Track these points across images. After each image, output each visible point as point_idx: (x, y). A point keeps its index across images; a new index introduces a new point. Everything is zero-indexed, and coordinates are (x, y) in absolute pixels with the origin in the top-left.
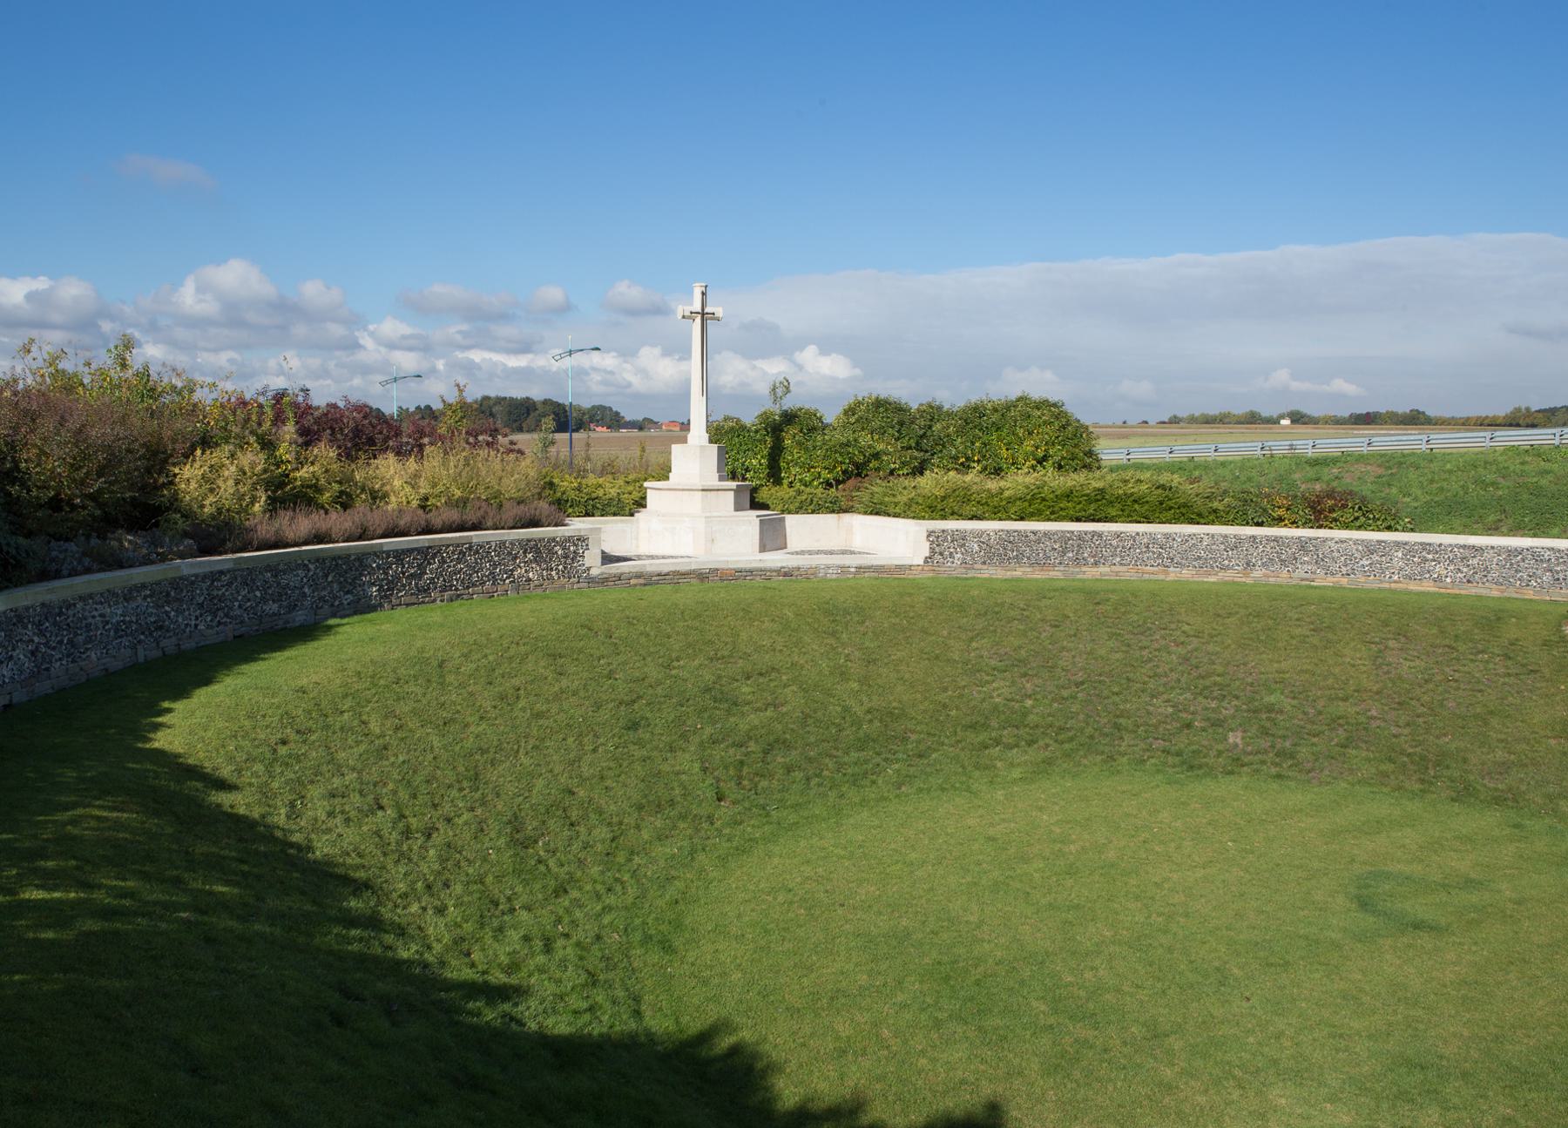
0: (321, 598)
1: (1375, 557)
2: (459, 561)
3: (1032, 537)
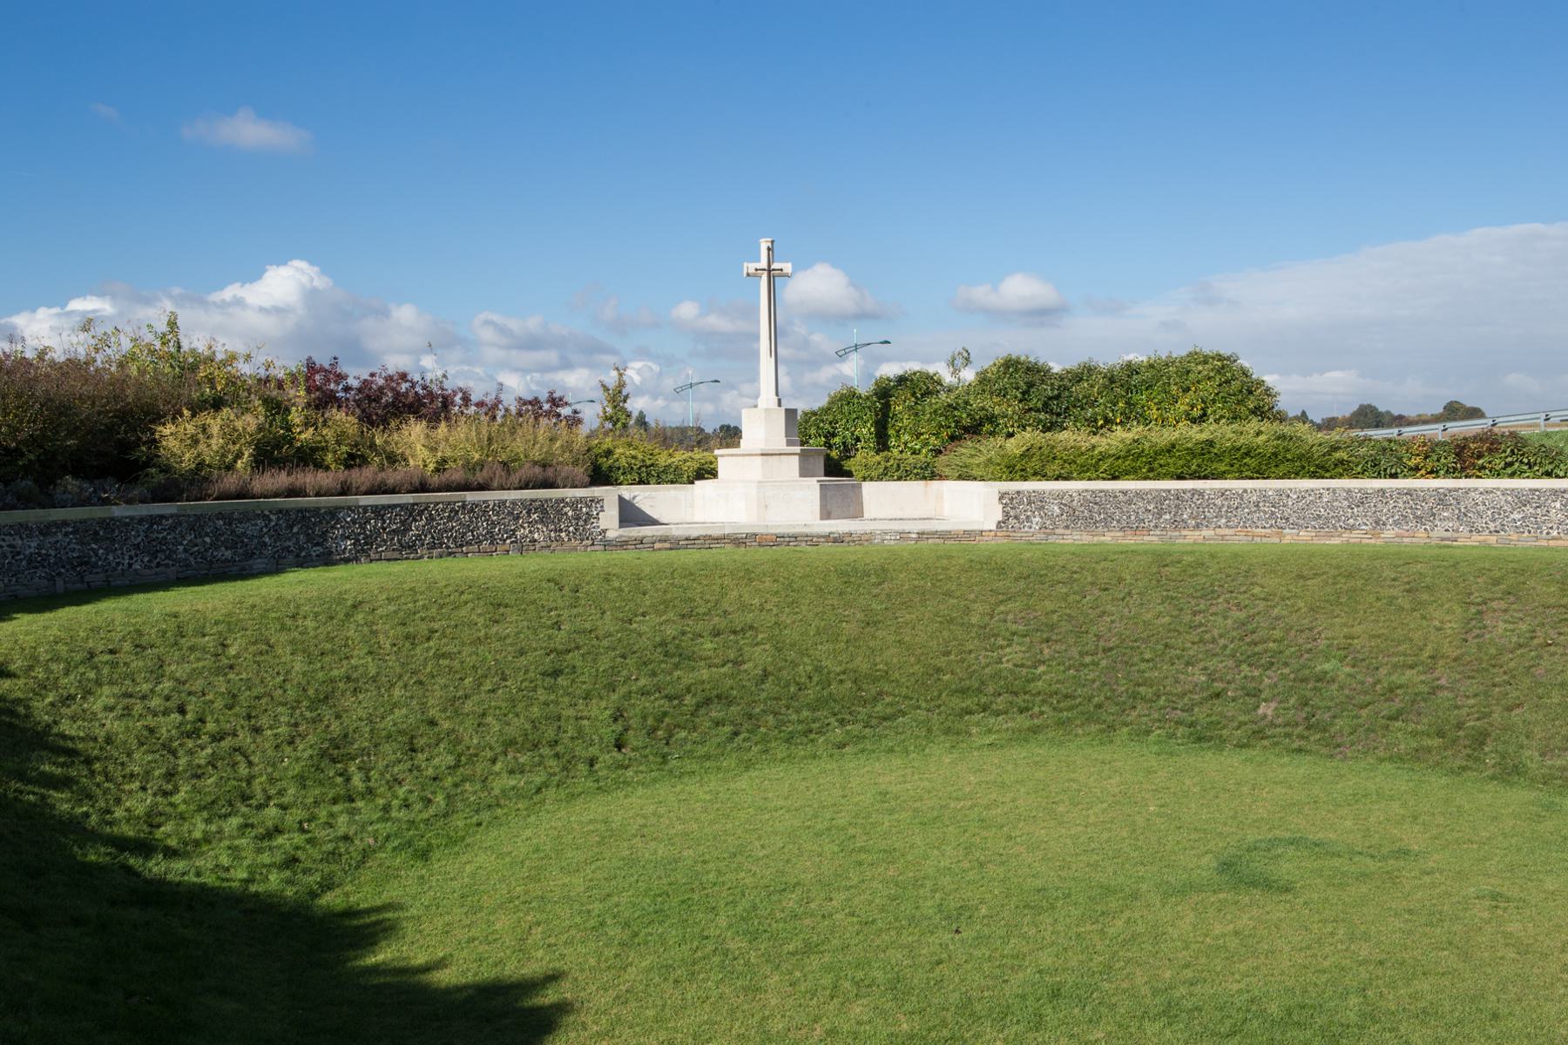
0: (287, 549)
1: (1529, 510)
2: (450, 519)
3: (1121, 497)
